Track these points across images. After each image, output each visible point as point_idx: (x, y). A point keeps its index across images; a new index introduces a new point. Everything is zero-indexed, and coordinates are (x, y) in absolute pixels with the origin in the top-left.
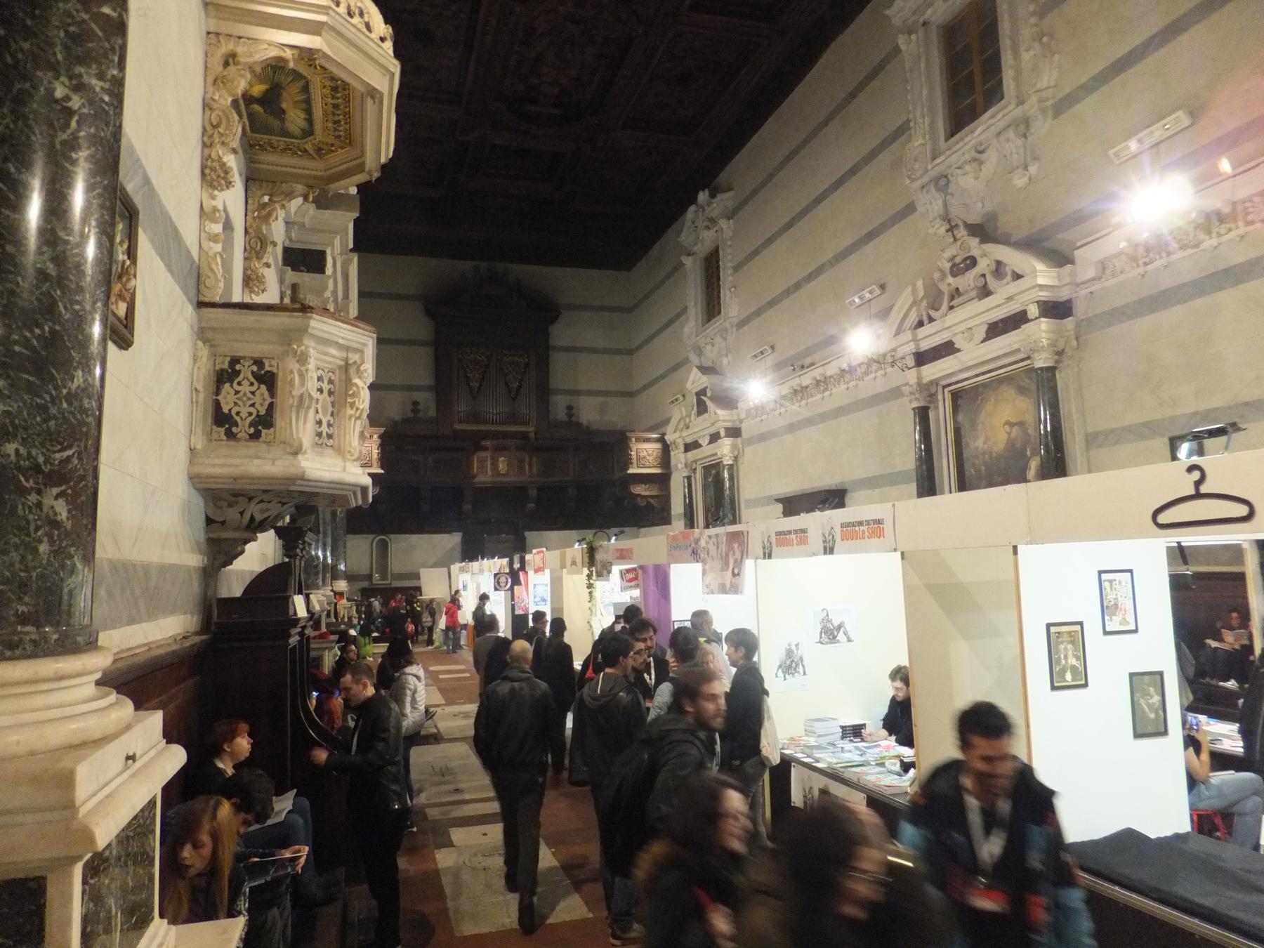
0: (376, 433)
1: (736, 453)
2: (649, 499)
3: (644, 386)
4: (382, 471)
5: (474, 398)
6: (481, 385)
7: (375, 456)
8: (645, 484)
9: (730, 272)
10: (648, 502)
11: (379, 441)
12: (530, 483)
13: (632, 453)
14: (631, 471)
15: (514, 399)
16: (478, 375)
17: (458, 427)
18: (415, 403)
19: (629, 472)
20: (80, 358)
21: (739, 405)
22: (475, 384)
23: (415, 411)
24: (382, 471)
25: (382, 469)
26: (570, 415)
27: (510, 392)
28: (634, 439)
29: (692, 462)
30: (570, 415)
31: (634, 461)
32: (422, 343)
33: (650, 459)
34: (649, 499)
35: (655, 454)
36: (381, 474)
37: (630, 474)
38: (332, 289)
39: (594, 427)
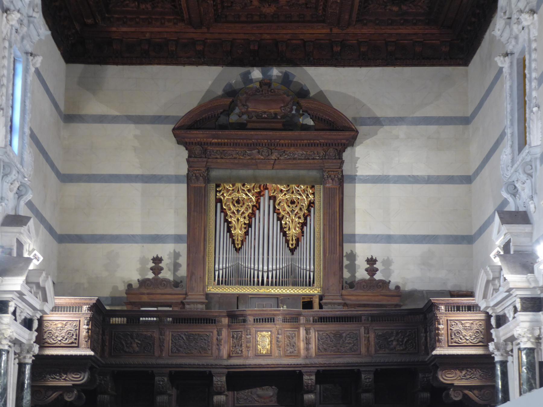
0: (85, 304)
1: (537, 333)
2: (466, 392)
3: (481, 228)
4: (92, 353)
5: (238, 250)
6: (247, 233)
7: (84, 333)
8: (461, 370)
9: (534, 84)
10: (465, 395)
11: (89, 314)
12: (305, 366)
13: (441, 327)
14: (438, 351)
15: (292, 251)
16: (242, 220)
17: (213, 289)
18: (157, 260)
19: (434, 353)
20: (220, 156)
21: (536, 266)
22: (238, 232)
23: (157, 270)
24: (92, 353)
25: (93, 350)
26: (372, 271)
27: (287, 241)
28: (443, 307)
29: (506, 341)
30: (372, 271)
31: (443, 338)
32: (176, 179)
33: (468, 335)
34: (466, 392)
35: (475, 327)
36: (90, 357)
37: (436, 356)
38: (526, 79)
39: (408, 287)
